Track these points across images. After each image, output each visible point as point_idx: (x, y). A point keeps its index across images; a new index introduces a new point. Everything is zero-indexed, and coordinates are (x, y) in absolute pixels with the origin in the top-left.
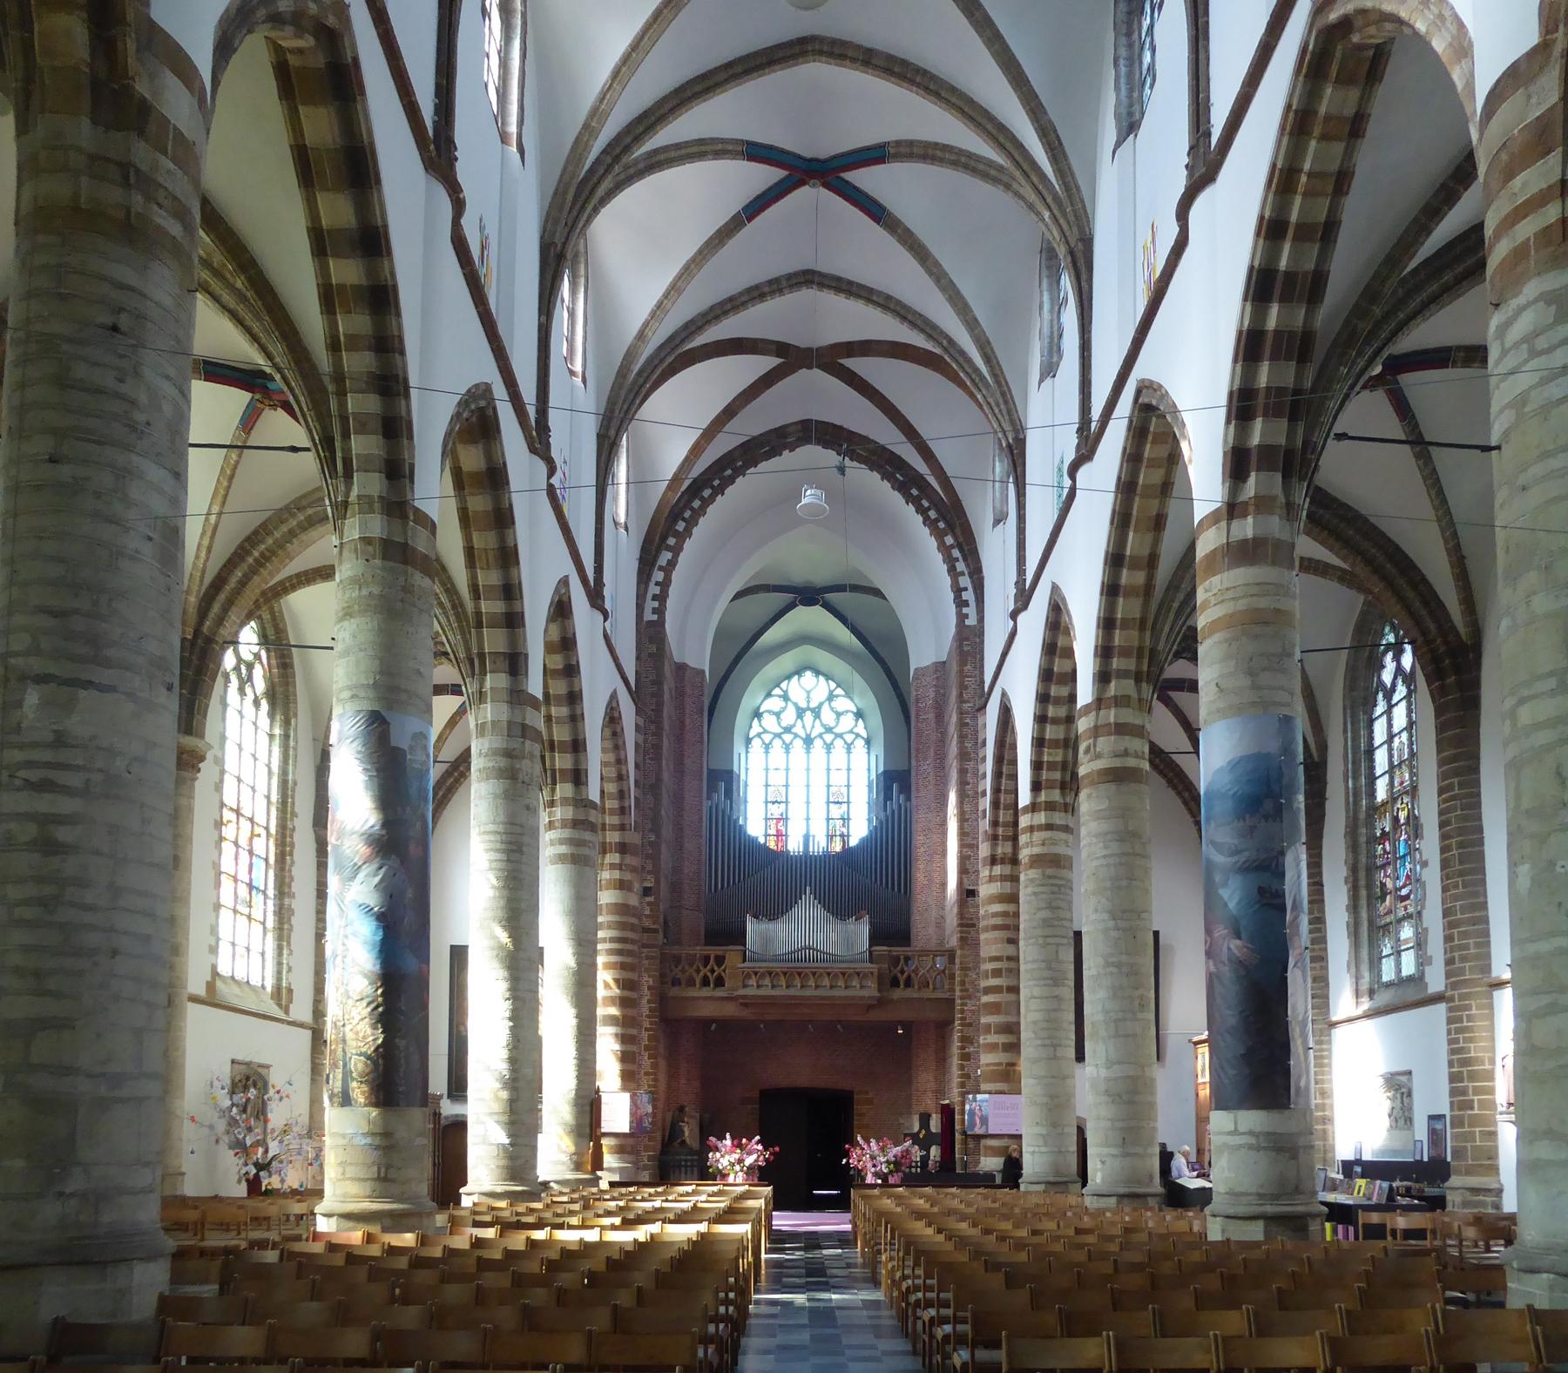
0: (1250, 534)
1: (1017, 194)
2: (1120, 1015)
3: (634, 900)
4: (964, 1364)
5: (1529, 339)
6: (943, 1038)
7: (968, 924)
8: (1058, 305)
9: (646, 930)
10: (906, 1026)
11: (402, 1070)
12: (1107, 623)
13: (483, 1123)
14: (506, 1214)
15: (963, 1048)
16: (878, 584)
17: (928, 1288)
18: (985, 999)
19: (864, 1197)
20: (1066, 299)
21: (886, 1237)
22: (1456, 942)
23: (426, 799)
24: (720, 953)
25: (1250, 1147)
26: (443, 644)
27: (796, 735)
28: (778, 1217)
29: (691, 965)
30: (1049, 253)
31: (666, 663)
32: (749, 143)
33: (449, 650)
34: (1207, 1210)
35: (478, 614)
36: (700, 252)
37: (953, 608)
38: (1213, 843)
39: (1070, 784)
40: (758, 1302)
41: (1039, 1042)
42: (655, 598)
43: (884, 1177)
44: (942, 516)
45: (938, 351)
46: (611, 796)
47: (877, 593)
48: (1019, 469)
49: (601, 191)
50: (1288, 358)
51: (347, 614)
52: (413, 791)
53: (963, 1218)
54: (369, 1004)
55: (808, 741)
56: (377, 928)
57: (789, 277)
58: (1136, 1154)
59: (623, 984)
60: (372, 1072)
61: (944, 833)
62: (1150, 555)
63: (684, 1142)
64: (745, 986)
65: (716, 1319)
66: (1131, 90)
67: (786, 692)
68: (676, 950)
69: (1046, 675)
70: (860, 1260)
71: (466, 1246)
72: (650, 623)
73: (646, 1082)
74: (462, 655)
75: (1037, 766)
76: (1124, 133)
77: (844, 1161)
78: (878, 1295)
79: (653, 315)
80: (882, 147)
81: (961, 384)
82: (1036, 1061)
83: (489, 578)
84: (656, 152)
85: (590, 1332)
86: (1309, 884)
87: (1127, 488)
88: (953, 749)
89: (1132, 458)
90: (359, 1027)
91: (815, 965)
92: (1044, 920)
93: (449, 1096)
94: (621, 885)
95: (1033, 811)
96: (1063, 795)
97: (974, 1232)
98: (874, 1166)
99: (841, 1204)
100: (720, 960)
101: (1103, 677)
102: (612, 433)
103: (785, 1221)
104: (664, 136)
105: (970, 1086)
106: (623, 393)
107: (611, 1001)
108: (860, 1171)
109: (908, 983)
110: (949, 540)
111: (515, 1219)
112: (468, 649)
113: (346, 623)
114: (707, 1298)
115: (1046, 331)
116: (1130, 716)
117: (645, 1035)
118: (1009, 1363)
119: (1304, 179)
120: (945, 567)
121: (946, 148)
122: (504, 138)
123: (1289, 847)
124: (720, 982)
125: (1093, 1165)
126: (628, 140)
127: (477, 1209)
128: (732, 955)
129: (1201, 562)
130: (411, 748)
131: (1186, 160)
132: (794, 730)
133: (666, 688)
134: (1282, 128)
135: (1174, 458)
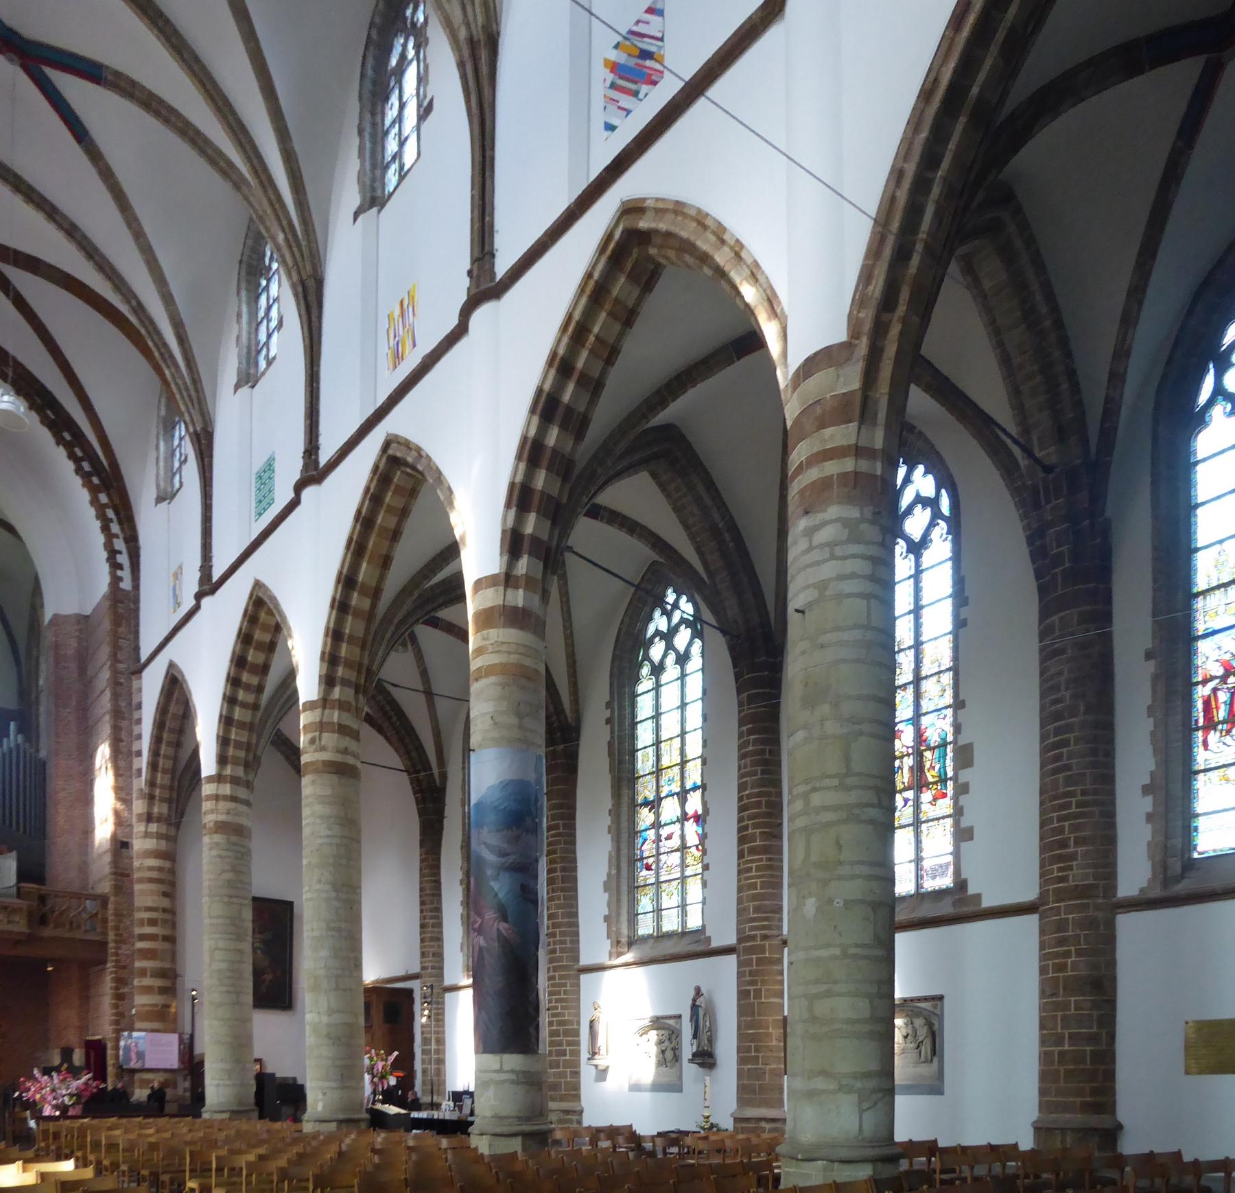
2: (340, 972)
5: (831, 545)
10: (56, 961)
18: (140, 945)
22: (558, 938)
25: (512, 1082)
37: (106, 568)
43: (64, 1109)
77: (17, 1094)
92: (229, 881)
105: (123, 1023)
110: (103, 498)
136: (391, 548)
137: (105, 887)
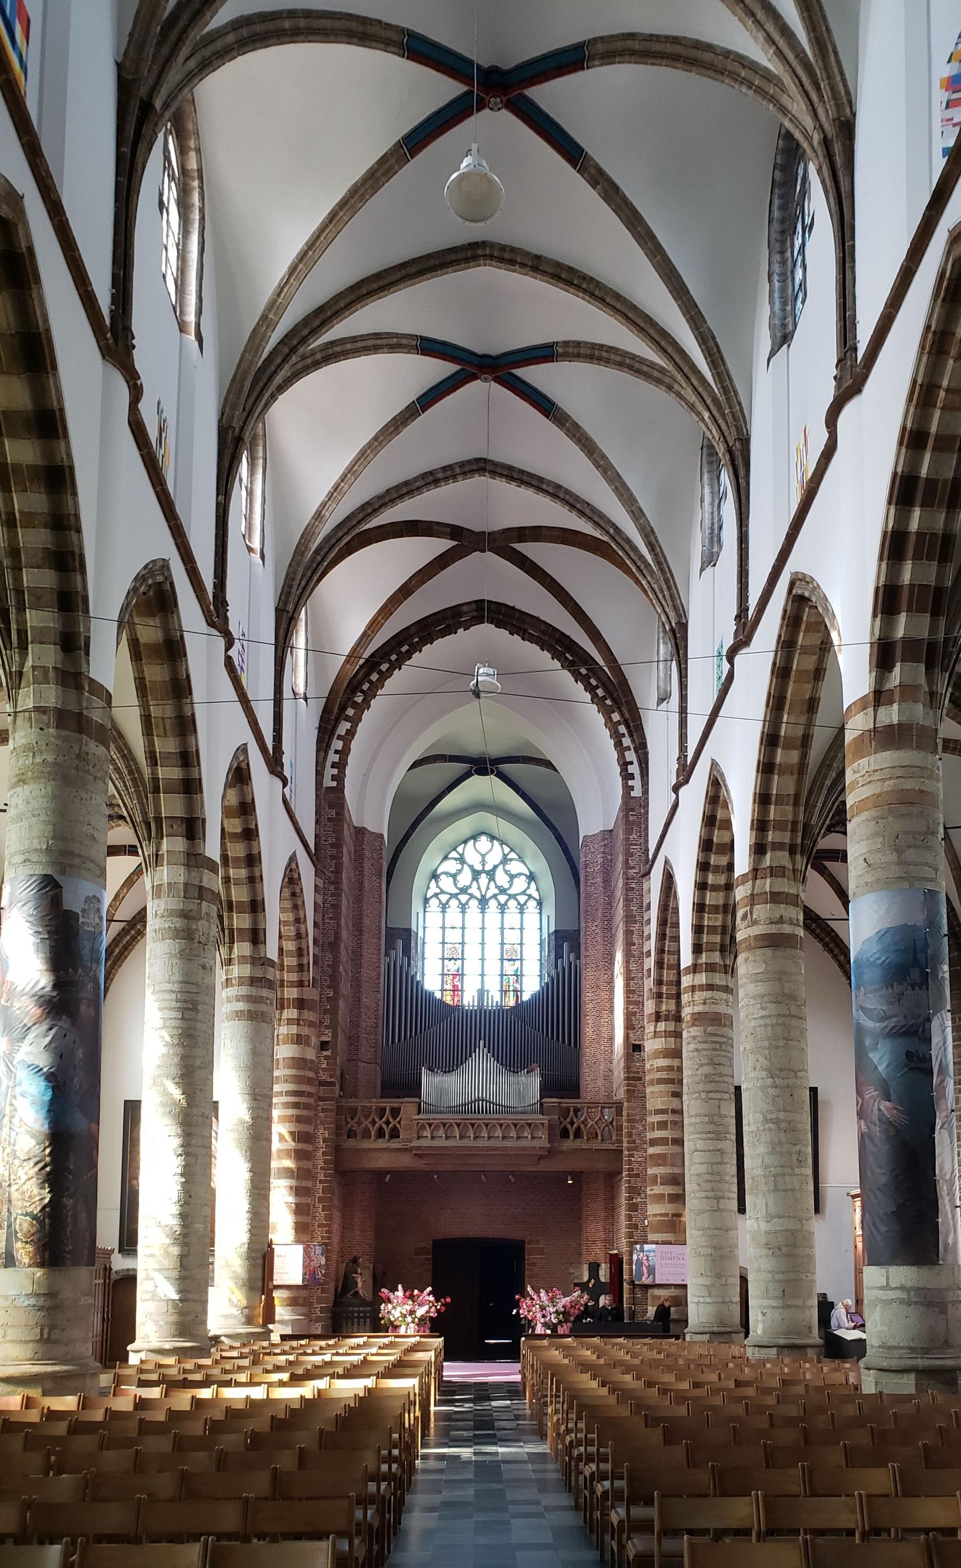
0: (895, 721)
1: (678, 395)
2: (779, 1170)
3: (311, 1054)
4: (621, 1522)
6: (612, 1187)
7: (634, 1078)
8: (718, 499)
9: (322, 1083)
10: (577, 1175)
11: (69, 1229)
12: (763, 799)
13: (153, 1279)
14: (173, 1372)
15: (631, 1198)
16: (549, 757)
17: (589, 1443)
18: (651, 1151)
19: (532, 1348)
20: (725, 493)
21: (551, 1389)
23: (98, 961)
24: (396, 1105)
25: (902, 1302)
26: (119, 806)
27: (472, 896)
28: (449, 1368)
29: (367, 1117)
30: (709, 450)
31: (346, 826)
32: (424, 339)
33: (125, 814)
34: (862, 1363)
35: (155, 780)
36: (376, 438)
38: (862, 1008)
39: (729, 947)
40: (425, 1457)
41: (703, 1194)
42: (334, 765)
43: (554, 1328)
44: (610, 694)
45: (605, 538)
46: (290, 954)
47: (548, 764)
48: (681, 652)
49: (278, 380)
50: (930, 558)
51: (21, 780)
52: (86, 953)
53: (628, 1369)
54: (36, 1164)
55: (483, 902)
56: (47, 1088)
57: (462, 464)
58: (796, 1306)
59: (298, 1136)
60: (38, 1231)
61: (612, 990)
62: (804, 736)
63: (357, 1292)
64: (419, 1138)
65: (377, 1477)
66: (784, 303)
67: (462, 855)
68: (352, 1103)
69: (706, 845)
70: (528, 1412)
71: (130, 1408)
72: (330, 789)
73: (319, 1233)
74: (138, 818)
75: (698, 929)
76: (778, 340)
77: (514, 1312)
78: (544, 1448)
79: (330, 496)
80: (551, 346)
81: (628, 571)
82: (700, 1213)
83: (167, 745)
84: (333, 343)
85: (247, 1499)
86: (954, 1047)
87: (781, 673)
88: (620, 912)
89: (787, 645)
90: (25, 1187)
91: (488, 1116)
93: (121, 1250)
94: (299, 1040)
95: (694, 972)
96: (723, 957)
97: (639, 1384)
98: (544, 1316)
99: (511, 1353)
100: (395, 1112)
101: (759, 849)
102: (290, 607)
103: (455, 1371)
104: (340, 330)
105: (637, 1237)
106: (301, 570)
107: (287, 1153)
108: (530, 1321)
109: (578, 1134)
110: (616, 717)
111: (182, 1377)
112: (145, 813)
113: (19, 789)
114: (369, 1460)
115: (707, 523)
116: (785, 886)
117: (320, 1187)
118: (662, 1522)
119: (942, 394)
120: (612, 742)
121: (611, 349)
122: (182, 327)
123: (935, 1014)
124: (395, 1134)
125: (754, 1316)
126: (305, 332)
127: (144, 1367)
128: (407, 1107)
129: (850, 745)
130: (84, 911)
131: (835, 372)
132: (470, 891)
133: (345, 850)
134: (922, 347)
135: (825, 646)
136: (815, 689)
137: (621, 1094)
